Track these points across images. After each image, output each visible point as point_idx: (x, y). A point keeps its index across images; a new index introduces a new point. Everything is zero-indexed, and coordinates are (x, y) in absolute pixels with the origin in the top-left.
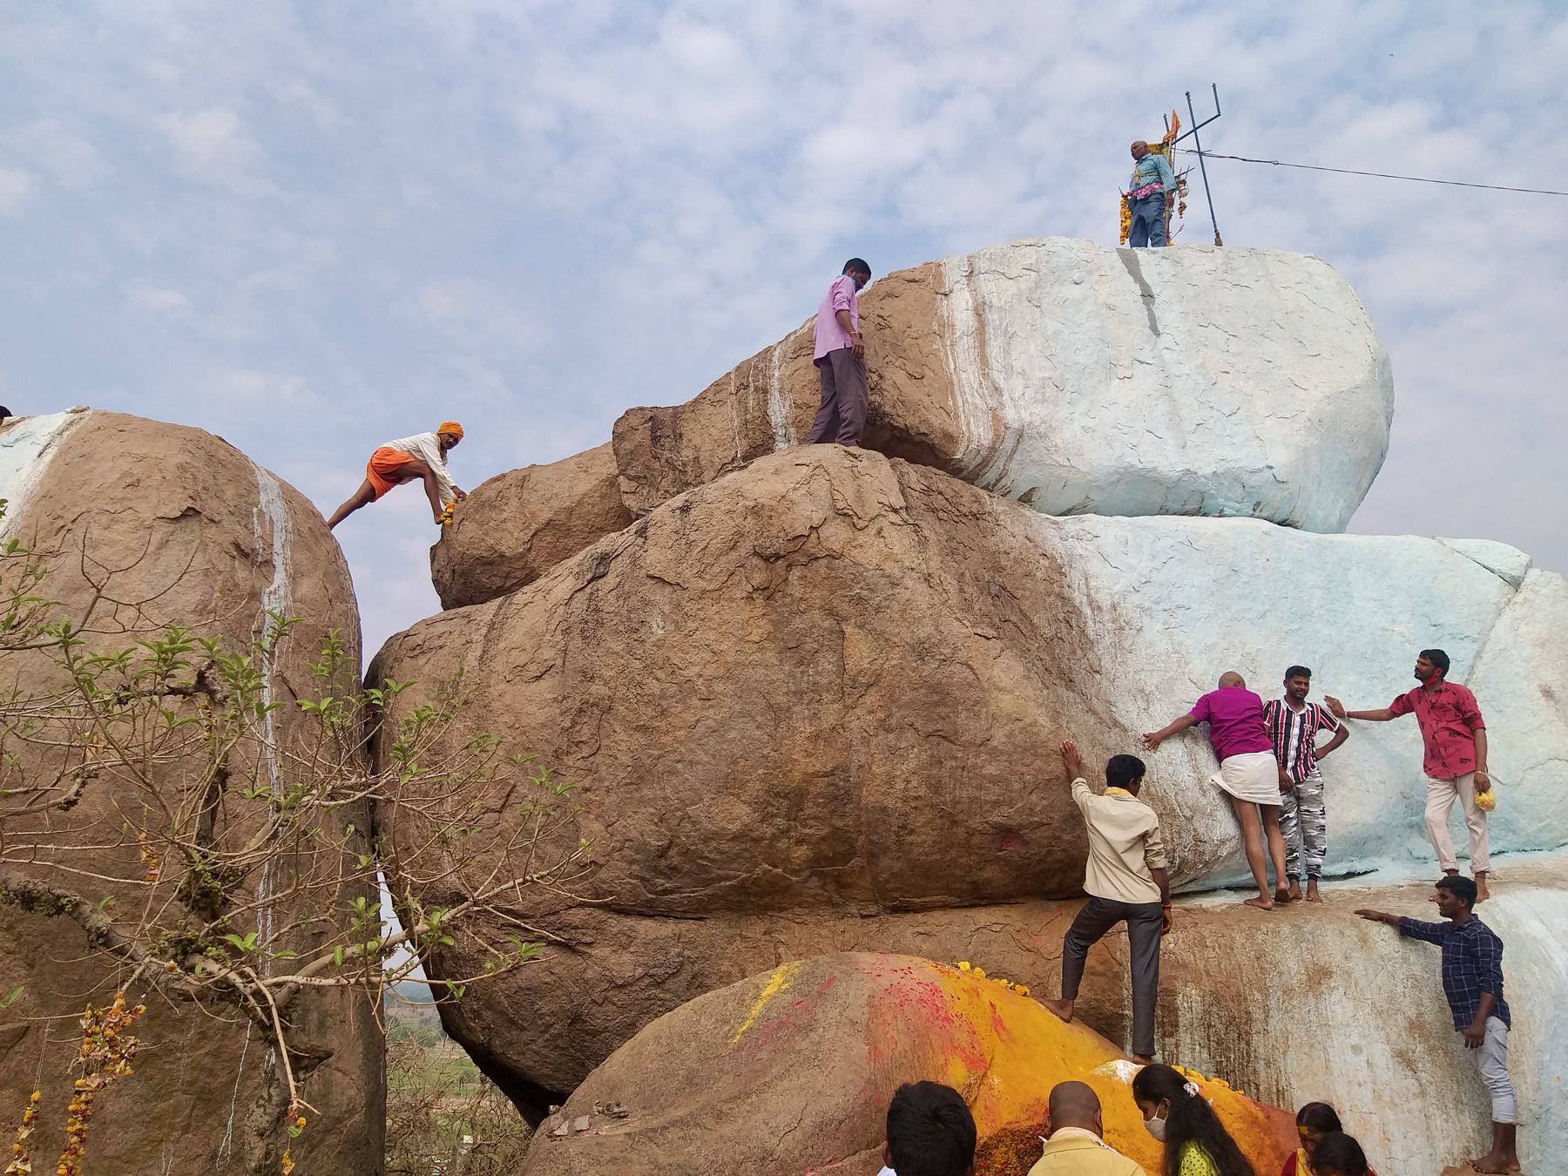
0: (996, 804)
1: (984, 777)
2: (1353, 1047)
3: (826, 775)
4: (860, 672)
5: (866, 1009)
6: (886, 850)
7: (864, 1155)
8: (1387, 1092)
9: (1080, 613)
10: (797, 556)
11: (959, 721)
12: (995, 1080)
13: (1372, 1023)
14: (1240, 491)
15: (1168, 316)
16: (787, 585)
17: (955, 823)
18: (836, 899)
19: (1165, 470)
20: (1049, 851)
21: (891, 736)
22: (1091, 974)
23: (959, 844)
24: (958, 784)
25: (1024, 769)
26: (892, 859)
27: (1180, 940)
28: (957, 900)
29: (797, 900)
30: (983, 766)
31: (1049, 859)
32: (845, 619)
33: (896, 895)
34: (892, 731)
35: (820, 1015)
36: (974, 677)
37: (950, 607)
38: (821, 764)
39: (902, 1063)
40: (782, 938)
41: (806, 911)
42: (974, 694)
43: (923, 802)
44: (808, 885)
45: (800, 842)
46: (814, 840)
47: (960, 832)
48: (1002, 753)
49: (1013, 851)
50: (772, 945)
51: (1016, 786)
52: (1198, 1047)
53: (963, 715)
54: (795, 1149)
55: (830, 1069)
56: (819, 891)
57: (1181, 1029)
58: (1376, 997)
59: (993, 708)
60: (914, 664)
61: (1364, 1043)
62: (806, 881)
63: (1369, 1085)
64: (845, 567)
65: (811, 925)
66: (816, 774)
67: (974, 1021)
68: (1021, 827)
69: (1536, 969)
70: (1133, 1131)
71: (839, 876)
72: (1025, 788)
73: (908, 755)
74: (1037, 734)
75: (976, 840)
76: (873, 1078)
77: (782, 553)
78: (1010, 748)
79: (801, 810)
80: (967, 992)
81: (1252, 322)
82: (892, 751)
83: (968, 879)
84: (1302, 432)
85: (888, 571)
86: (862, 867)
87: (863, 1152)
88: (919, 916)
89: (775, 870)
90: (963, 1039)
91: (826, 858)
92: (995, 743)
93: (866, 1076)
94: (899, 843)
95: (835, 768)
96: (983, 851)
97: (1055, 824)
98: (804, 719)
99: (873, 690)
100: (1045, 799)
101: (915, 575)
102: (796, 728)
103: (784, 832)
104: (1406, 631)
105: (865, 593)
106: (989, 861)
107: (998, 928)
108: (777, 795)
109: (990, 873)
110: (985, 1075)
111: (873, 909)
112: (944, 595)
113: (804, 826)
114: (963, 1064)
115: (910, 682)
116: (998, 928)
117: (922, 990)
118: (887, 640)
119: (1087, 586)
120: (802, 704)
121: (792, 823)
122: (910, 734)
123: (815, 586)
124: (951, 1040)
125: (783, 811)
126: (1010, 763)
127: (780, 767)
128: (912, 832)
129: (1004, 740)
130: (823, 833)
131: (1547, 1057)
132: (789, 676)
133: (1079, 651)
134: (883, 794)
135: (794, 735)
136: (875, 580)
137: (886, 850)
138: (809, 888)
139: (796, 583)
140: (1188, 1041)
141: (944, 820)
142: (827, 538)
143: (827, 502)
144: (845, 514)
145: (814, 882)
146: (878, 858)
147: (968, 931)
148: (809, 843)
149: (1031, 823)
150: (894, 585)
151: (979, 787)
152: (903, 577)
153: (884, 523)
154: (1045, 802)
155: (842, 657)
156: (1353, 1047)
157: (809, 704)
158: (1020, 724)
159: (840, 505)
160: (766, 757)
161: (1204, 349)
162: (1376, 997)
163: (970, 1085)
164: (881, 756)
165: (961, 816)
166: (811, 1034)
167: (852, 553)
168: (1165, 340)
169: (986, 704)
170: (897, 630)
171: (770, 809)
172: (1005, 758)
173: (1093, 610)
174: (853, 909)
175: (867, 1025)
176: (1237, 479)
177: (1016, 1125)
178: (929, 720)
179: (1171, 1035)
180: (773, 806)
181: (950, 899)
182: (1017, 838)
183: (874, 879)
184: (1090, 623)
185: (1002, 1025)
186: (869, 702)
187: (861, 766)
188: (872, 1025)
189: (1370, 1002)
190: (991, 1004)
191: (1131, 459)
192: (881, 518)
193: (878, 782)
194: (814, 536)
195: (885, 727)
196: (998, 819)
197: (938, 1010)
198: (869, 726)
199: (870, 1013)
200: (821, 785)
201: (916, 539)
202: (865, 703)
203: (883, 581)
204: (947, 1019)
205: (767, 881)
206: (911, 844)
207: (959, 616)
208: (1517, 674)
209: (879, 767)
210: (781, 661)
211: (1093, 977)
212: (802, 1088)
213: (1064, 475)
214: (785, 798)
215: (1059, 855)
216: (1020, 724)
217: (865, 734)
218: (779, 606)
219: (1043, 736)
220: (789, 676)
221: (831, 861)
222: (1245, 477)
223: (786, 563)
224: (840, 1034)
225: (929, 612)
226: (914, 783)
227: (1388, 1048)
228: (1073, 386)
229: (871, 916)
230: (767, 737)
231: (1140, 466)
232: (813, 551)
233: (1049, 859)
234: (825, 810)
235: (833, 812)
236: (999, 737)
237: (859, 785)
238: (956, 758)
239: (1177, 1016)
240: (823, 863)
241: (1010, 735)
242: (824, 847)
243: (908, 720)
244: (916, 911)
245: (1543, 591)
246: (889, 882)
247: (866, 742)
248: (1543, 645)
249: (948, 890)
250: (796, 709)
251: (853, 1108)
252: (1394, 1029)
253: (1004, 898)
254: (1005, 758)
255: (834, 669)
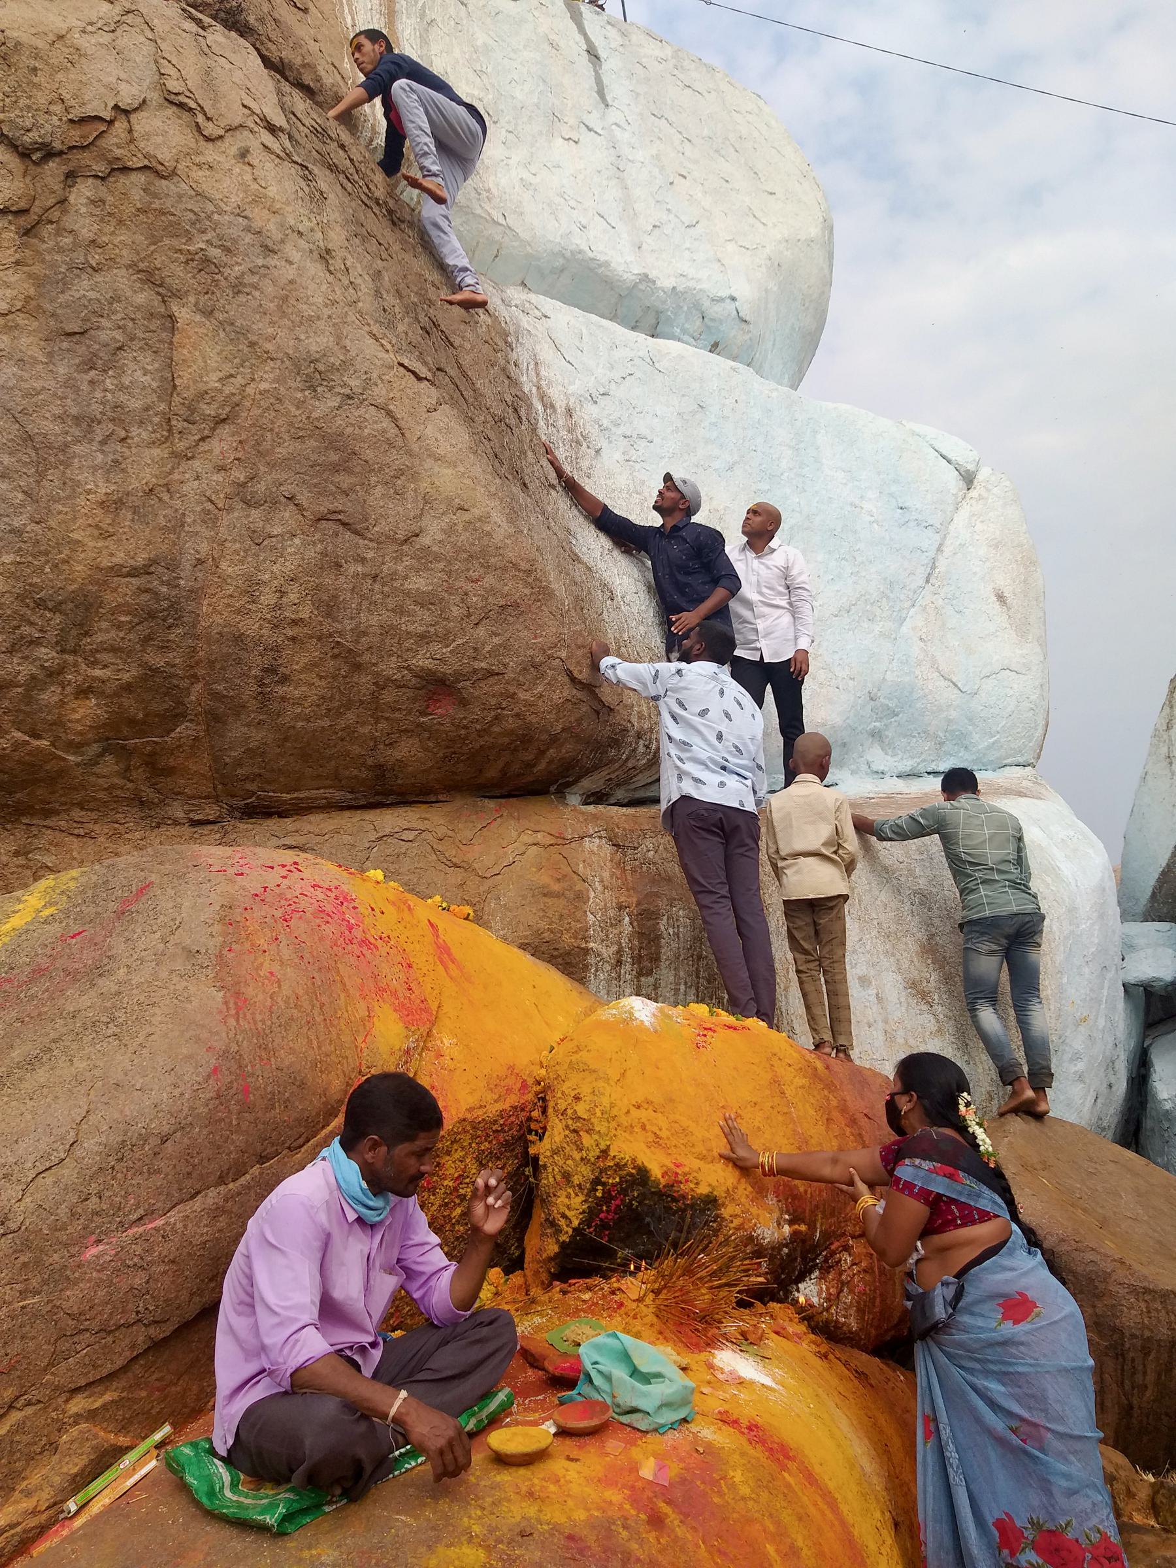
0: (424, 638)
1: (408, 594)
2: (860, 978)
3: (134, 573)
4: (202, 395)
5: (217, 928)
6: (239, 709)
7: (212, 1196)
8: (901, 1033)
9: (530, 406)
10: (85, 158)
11: (371, 500)
12: (445, 1041)
13: (881, 948)
14: (698, 322)
15: (617, 89)
16: (65, 212)
17: (357, 667)
18: (148, 793)
19: (620, 269)
20: (496, 718)
21: (255, 514)
22: (545, 895)
23: (362, 703)
24: (365, 603)
25: (469, 587)
26: (248, 725)
27: (661, 847)
28: (349, 796)
29: (78, 797)
30: (406, 577)
31: (496, 729)
32: (178, 295)
33: (252, 787)
34: (257, 505)
35: (118, 946)
36: (395, 431)
37: (360, 312)
38: (127, 553)
39: (292, 1019)
40: (49, 860)
41: (94, 815)
42: (397, 460)
43: (306, 630)
44: (96, 770)
45: (83, 692)
46: (110, 688)
47: (364, 681)
48: (437, 558)
49: (445, 714)
50: (29, 873)
51: (456, 612)
52: (682, 987)
53: (379, 491)
54: (58, 1204)
55: (141, 1039)
56: (117, 781)
57: (663, 965)
58: (882, 917)
59: (424, 485)
60: (299, 395)
61: (872, 972)
62: (94, 762)
63: (881, 1025)
64: (180, 196)
65: (102, 839)
66: (117, 571)
67: (409, 948)
68: (459, 676)
69: (1049, 880)
70: (671, 1100)
71: (152, 754)
72: (469, 615)
73: (284, 548)
74: (489, 534)
75: (388, 696)
76: (234, 1048)
77: (57, 145)
78: (448, 550)
79: (87, 634)
80: (394, 904)
81: (706, 132)
82: (257, 538)
83: (370, 762)
84: (764, 269)
85: (257, 224)
86: (196, 739)
87: (212, 1193)
88: (288, 823)
89: (36, 743)
90: (393, 975)
91: (132, 722)
92: (426, 540)
93: (219, 1045)
94: (263, 697)
95: (153, 562)
96: (397, 715)
97: (510, 675)
98: (95, 469)
99: (225, 431)
100: (497, 635)
101: (302, 243)
102: (78, 484)
103: (54, 674)
104: (874, 510)
105: (214, 253)
106: (406, 731)
107: (410, 835)
108: (40, 604)
109: (407, 750)
110: (429, 1034)
111: (211, 811)
112: (351, 290)
113: (93, 664)
114: (396, 1015)
115: (291, 424)
116: (410, 835)
117: (321, 897)
118: (252, 344)
119: (538, 374)
120: (91, 441)
121: (70, 658)
122: (288, 513)
123: (120, 222)
124: (375, 977)
125: (51, 636)
126: (449, 574)
127: (46, 553)
128: (285, 679)
129: (440, 536)
130: (126, 677)
131: (1065, 980)
132: (66, 385)
133: (530, 454)
134: (238, 612)
135: (73, 495)
136: (234, 232)
137: (239, 709)
138: (98, 776)
139: (83, 210)
140: (672, 979)
141: (339, 661)
142: (147, 136)
143: (150, 76)
144: (181, 105)
145: (109, 765)
146: (225, 723)
147: (365, 841)
148: (101, 694)
149: (475, 671)
150: (268, 250)
151: (400, 611)
152: (283, 241)
153: (243, 139)
154: (496, 640)
155: (170, 363)
156: (860, 978)
157: (103, 442)
158: (467, 516)
159: (173, 85)
160: (17, 532)
161: (658, 142)
162: (882, 917)
163: (407, 1052)
164: (238, 546)
165: (367, 657)
166: (101, 982)
167: (193, 174)
168: (613, 115)
169: (415, 477)
170: (270, 330)
171: (26, 629)
172: (440, 566)
173: (545, 406)
174: (177, 810)
175: (220, 956)
176: (697, 306)
177: (480, 1112)
178: (322, 493)
179: (649, 973)
180: (32, 624)
181: (337, 795)
182: (450, 695)
183: (216, 759)
184: (542, 423)
185: (449, 954)
186: (217, 451)
187: (200, 562)
188: (230, 955)
189: (875, 922)
190: (432, 925)
191: (579, 241)
192: (246, 133)
193: (230, 590)
194: (120, 125)
195: (243, 495)
196: (426, 663)
197: (350, 928)
198: (216, 492)
199: (225, 934)
200: (125, 590)
201: (307, 189)
202: (210, 451)
203: (249, 238)
204: (365, 942)
205: (19, 762)
206: (283, 699)
207: (375, 329)
208: (975, 573)
209: (233, 564)
210: (50, 355)
211: (546, 899)
212: (78, 1080)
213: (498, 238)
214: (54, 610)
215: (511, 723)
216: (467, 516)
217: (209, 506)
218: (50, 251)
219: (498, 537)
220: (66, 385)
221: (139, 727)
222: (706, 303)
223: (65, 169)
224: (164, 975)
225: (326, 312)
226: (293, 597)
227: (899, 978)
228: (509, 122)
229: (209, 822)
230: (20, 496)
231: (590, 254)
232: (118, 152)
233: (496, 729)
234: (132, 636)
235: (147, 639)
236: (433, 533)
237: (195, 594)
238: (363, 560)
239: (659, 947)
240: (126, 731)
241: (451, 530)
242: (128, 702)
243: (286, 489)
244: (281, 815)
245: (995, 490)
246: (240, 765)
247: (209, 519)
248: (997, 546)
249: (337, 780)
250: (78, 449)
251: (192, 1109)
252: (905, 954)
253: (417, 795)
254: (440, 566)
255: (155, 385)
